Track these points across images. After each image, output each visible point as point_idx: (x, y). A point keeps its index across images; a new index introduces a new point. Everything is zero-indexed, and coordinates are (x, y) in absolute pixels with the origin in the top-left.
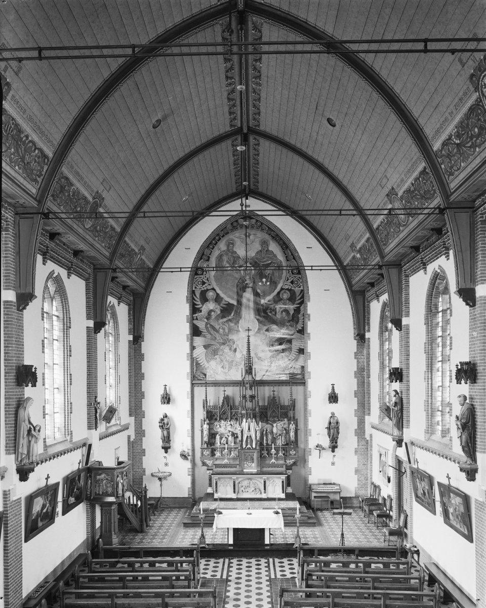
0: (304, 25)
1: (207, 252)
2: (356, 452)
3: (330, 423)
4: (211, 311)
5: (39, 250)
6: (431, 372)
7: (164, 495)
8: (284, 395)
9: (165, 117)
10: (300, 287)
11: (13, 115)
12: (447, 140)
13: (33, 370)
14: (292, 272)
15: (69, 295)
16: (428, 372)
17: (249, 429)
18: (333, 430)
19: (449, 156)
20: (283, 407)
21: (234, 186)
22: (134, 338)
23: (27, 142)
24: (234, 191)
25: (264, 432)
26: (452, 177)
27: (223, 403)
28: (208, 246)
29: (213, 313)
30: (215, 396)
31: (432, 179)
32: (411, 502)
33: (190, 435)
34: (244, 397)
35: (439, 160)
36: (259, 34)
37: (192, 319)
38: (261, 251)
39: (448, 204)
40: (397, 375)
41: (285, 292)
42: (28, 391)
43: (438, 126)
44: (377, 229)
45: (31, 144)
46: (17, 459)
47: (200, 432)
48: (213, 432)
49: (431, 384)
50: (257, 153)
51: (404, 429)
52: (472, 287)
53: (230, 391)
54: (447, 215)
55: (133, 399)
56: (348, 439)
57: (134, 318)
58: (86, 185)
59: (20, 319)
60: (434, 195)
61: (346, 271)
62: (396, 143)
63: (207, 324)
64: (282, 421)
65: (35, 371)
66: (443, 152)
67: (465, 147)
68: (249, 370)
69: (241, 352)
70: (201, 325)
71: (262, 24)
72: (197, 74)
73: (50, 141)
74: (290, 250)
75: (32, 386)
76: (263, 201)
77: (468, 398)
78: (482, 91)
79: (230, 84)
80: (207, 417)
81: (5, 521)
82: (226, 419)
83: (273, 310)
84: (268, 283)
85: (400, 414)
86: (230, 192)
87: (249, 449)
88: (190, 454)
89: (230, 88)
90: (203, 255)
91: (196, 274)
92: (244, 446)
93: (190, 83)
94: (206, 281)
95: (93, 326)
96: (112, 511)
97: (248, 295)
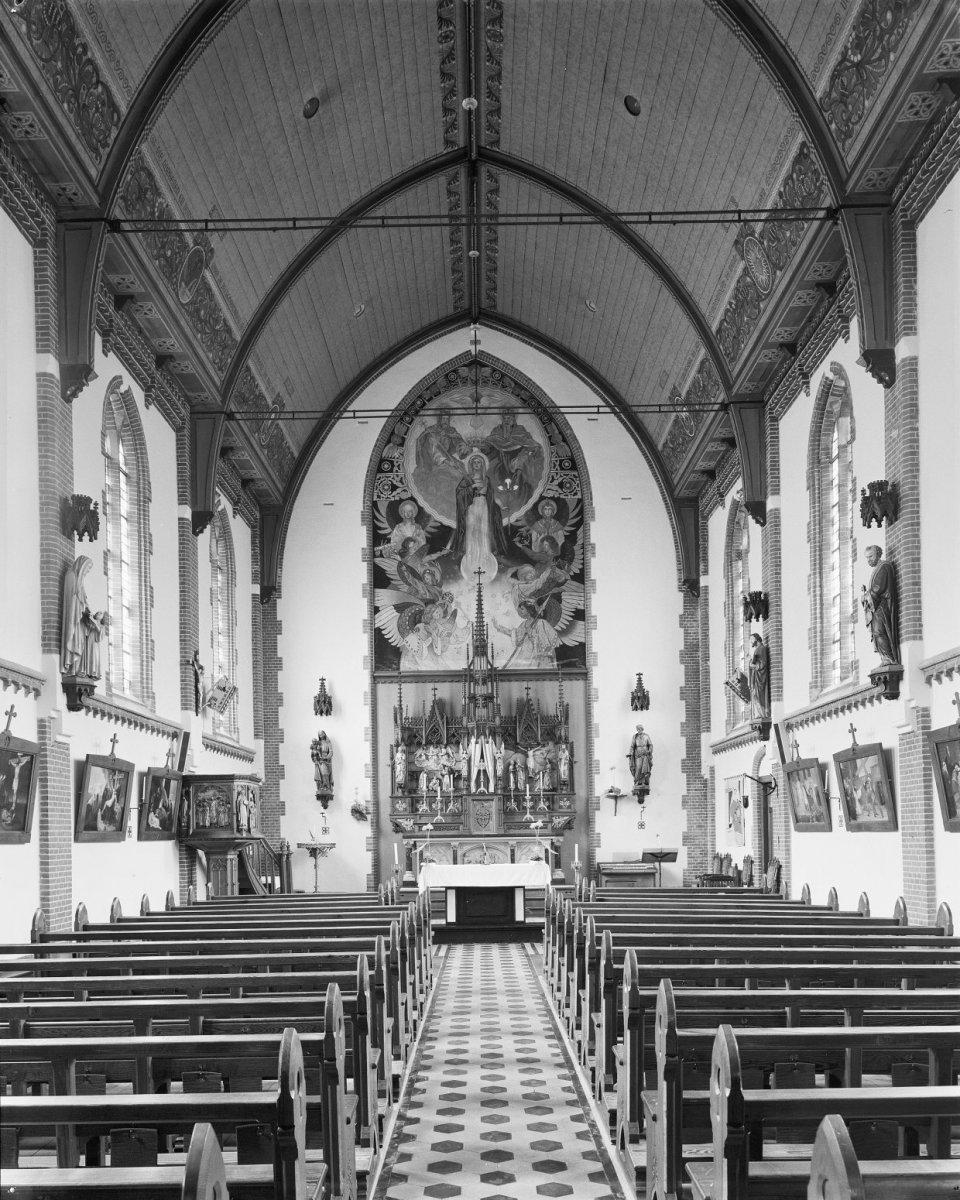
1: (400, 429)
2: (684, 802)
3: (635, 747)
4: (408, 540)
6: (821, 573)
7: (322, 890)
8: (548, 695)
9: (327, 96)
10: (576, 494)
12: (840, 63)
13: (92, 507)
14: (560, 465)
15: (146, 431)
16: (815, 574)
17: (482, 757)
18: (640, 759)
20: (545, 719)
21: (451, 298)
22: (263, 589)
23: (84, 58)
24: (451, 311)
25: (511, 767)
27: (433, 712)
29: (411, 544)
30: (415, 700)
31: (818, 165)
32: (787, 829)
33: (370, 774)
34: (473, 698)
35: (826, 115)
40: (759, 606)
41: (548, 504)
42: (82, 547)
44: (719, 331)
45: (89, 68)
46: (63, 663)
47: (390, 769)
48: (414, 769)
49: (821, 596)
51: (773, 704)
52: (888, 347)
53: (445, 691)
54: (843, 221)
55: (261, 706)
56: (668, 779)
57: (262, 553)
58: (181, 201)
59: (67, 417)
60: (819, 196)
61: (660, 462)
63: (400, 564)
64: (544, 746)
66: (834, 95)
68: (481, 648)
69: (465, 616)
70: (390, 566)
74: (557, 425)
75: (91, 540)
76: (506, 333)
77: (884, 552)
80: (403, 739)
81: (41, 774)
82: (438, 743)
83: (526, 538)
84: (516, 487)
85: (764, 676)
86: (443, 314)
87: (483, 794)
88: (371, 809)
89: (444, 46)
90: (392, 436)
91: (380, 470)
92: (473, 790)
94: (399, 484)
96: (229, 862)
97: (478, 510)
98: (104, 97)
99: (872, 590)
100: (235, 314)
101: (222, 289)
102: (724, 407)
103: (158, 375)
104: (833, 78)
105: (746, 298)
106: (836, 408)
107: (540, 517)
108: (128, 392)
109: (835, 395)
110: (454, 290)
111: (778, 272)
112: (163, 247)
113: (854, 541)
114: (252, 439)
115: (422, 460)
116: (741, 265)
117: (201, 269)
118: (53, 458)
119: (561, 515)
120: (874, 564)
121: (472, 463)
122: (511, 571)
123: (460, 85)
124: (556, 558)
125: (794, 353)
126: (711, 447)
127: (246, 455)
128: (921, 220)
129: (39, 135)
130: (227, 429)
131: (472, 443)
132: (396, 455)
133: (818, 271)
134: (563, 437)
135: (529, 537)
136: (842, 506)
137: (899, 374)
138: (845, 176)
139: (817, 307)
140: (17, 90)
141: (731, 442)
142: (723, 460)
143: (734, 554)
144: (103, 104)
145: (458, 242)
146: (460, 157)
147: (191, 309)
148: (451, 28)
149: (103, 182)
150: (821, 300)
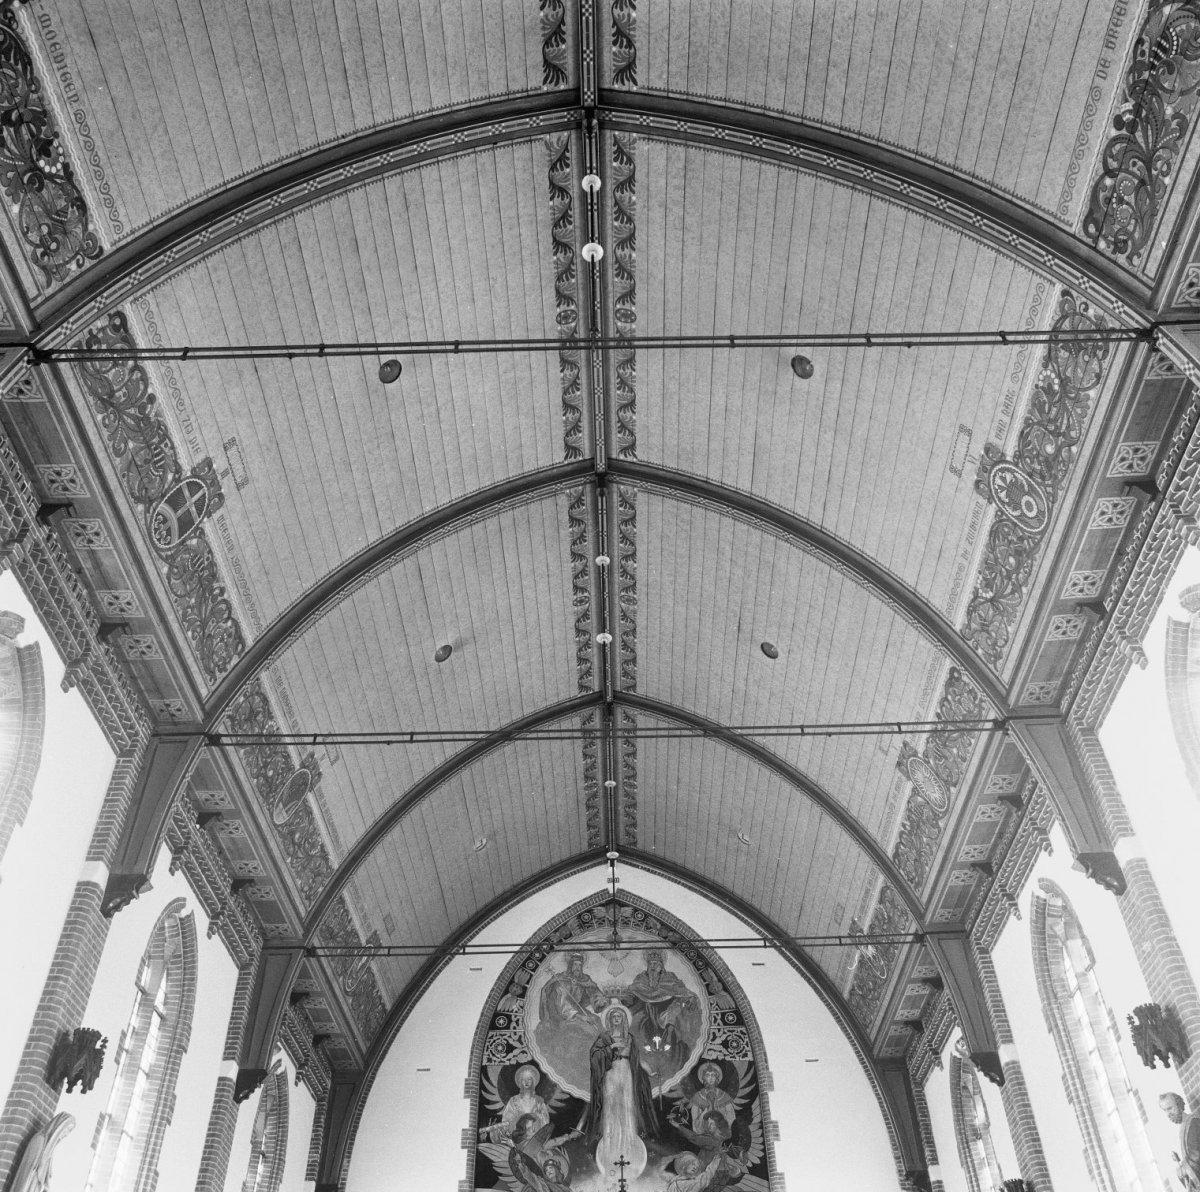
0: (705, 485)
4: (525, 1118)
5: (170, 837)
9: (460, 644)
10: (745, 1055)
11: (212, 545)
12: (973, 601)
13: (98, 1046)
14: (723, 1019)
19: (984, 627)
21: (586, 835)
23: (220, 598)
24: (585, 847)
26: (1001, 661)
28: (524, 965)
29: (530, 1124)
31: (973, 684)
35: (970, 643)
36: (631, 548)
37: (476, 1140)
38: (647, 974)
39: (1008, 711)
41: (710, 1069)
42: (70, 1101)
43: (951, 585)
44: (896, 855)
50: (630, 582)
54: (1013, 729)
57: (326, 1137)
59: (101, 934)
61: (849, 1013)
62: (890, 649)
65: (103, 1046)
66: (973, 626)
67: (1004, 597)
70: (499, 1155)
71: (635, 495)
72: (524, 573)
73: (255, 616)
75: (83, 1091)
77: (1185, 1101)
78: (1000, 499)
79: (581, 601)
83: (684, 1115)
84: (667, 1047)
86: (575, 852)
89: (580, 608)
90: (511, 985)
91: (493, 1026)
93: (511, 589)
95: (234, 1079)
97: (620, 1077)
98: (233, 630)
99: (1188, 1159)
100: (336, 840)
101: (325, 813)
102: (919, 938)
103: (231, 902)
104: (969, 613)
105: (920, 819)
106: (1060, 929)
107: (700, 1086)
108: (190, 917)
109: (1053, 916)
110: (589, 826)
111: (952, 789)
112: (266, 765)
113: (1136, 1093)
114: (335, 984)
115: (546, 1013)
116: (908, 786)
117: (303, 792)
118: (66, 981)
119: (728, 1083)
120: (1179, 1119)
121: (611, 1017)
122: (666, 1161)
123: (574, 148)
124: (727, 1142)
125: (991, 874)
126: (911, 990)
127: (323, 1004)
128: (1101, 725)
129: (154, 656)
130: (304, 968)
131: (609, 995)
132: (515, 1007)
133: (996, 783)
134: (723, 984)
135: (688, 1114)
136: (1102, 1050)
137: (1129, 879)
138: (1004, 692)
139: (1005, 824)
140: (143, 616)
141: (936, 983)
142: (929, 1008)
143: (968, 1134)
144: (229, 636)
145: (593, 778)
146: (597, 699)
147: (285, 830)
148: (573, 307)
149: (212, 701)
150: (1009, 815)
